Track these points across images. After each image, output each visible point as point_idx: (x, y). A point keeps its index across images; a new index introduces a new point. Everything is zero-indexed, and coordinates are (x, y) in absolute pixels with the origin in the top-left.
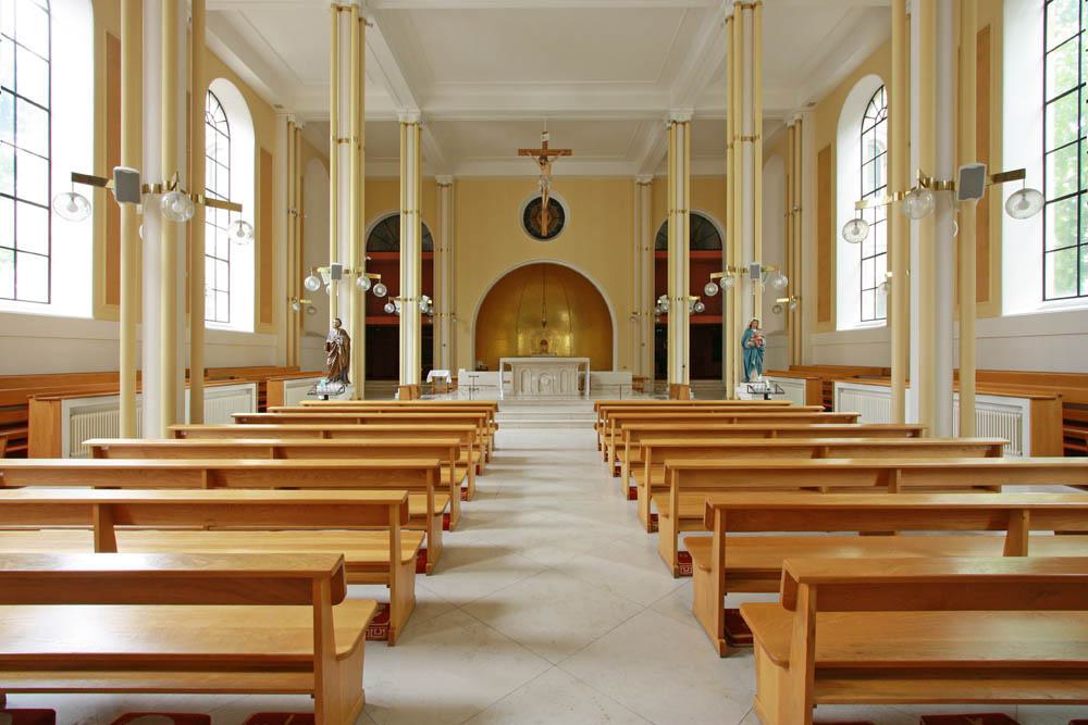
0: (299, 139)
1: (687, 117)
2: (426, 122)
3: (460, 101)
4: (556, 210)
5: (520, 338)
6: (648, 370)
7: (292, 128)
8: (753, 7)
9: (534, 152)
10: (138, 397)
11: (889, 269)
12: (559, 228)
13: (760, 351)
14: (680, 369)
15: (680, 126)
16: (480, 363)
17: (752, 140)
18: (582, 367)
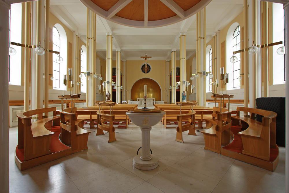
0: (79, 40)
1: (175, 50)
2: (122, 51)
3: (128, 47)
4: (149, 67)
5: (141, 94)
6: (169, 101)
7: (77, 36)
8: (184, 36)
9: (144, 57)
10: (29, 106)
11: (213, 81)
12: (149, 71)
13: (185, 96)
14: (174, 100)
15: (174, 52)
16: (132, 100)
17: (184, 59)
18: (153, 100)
